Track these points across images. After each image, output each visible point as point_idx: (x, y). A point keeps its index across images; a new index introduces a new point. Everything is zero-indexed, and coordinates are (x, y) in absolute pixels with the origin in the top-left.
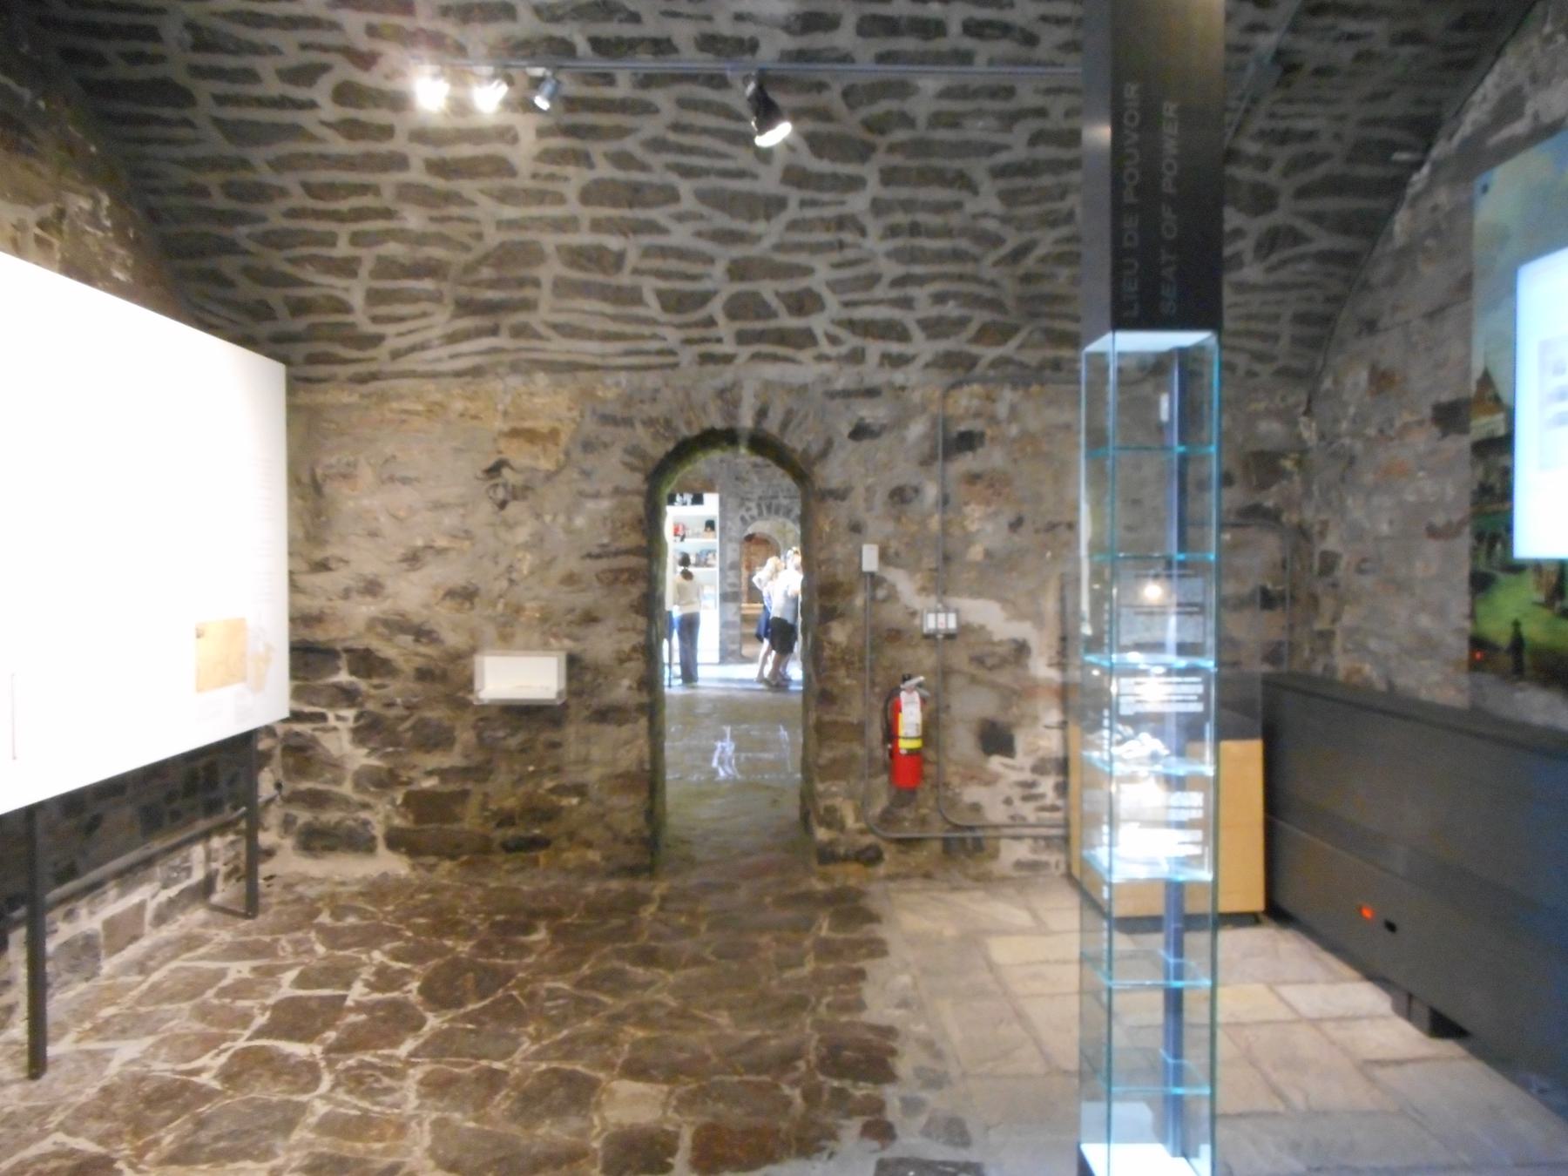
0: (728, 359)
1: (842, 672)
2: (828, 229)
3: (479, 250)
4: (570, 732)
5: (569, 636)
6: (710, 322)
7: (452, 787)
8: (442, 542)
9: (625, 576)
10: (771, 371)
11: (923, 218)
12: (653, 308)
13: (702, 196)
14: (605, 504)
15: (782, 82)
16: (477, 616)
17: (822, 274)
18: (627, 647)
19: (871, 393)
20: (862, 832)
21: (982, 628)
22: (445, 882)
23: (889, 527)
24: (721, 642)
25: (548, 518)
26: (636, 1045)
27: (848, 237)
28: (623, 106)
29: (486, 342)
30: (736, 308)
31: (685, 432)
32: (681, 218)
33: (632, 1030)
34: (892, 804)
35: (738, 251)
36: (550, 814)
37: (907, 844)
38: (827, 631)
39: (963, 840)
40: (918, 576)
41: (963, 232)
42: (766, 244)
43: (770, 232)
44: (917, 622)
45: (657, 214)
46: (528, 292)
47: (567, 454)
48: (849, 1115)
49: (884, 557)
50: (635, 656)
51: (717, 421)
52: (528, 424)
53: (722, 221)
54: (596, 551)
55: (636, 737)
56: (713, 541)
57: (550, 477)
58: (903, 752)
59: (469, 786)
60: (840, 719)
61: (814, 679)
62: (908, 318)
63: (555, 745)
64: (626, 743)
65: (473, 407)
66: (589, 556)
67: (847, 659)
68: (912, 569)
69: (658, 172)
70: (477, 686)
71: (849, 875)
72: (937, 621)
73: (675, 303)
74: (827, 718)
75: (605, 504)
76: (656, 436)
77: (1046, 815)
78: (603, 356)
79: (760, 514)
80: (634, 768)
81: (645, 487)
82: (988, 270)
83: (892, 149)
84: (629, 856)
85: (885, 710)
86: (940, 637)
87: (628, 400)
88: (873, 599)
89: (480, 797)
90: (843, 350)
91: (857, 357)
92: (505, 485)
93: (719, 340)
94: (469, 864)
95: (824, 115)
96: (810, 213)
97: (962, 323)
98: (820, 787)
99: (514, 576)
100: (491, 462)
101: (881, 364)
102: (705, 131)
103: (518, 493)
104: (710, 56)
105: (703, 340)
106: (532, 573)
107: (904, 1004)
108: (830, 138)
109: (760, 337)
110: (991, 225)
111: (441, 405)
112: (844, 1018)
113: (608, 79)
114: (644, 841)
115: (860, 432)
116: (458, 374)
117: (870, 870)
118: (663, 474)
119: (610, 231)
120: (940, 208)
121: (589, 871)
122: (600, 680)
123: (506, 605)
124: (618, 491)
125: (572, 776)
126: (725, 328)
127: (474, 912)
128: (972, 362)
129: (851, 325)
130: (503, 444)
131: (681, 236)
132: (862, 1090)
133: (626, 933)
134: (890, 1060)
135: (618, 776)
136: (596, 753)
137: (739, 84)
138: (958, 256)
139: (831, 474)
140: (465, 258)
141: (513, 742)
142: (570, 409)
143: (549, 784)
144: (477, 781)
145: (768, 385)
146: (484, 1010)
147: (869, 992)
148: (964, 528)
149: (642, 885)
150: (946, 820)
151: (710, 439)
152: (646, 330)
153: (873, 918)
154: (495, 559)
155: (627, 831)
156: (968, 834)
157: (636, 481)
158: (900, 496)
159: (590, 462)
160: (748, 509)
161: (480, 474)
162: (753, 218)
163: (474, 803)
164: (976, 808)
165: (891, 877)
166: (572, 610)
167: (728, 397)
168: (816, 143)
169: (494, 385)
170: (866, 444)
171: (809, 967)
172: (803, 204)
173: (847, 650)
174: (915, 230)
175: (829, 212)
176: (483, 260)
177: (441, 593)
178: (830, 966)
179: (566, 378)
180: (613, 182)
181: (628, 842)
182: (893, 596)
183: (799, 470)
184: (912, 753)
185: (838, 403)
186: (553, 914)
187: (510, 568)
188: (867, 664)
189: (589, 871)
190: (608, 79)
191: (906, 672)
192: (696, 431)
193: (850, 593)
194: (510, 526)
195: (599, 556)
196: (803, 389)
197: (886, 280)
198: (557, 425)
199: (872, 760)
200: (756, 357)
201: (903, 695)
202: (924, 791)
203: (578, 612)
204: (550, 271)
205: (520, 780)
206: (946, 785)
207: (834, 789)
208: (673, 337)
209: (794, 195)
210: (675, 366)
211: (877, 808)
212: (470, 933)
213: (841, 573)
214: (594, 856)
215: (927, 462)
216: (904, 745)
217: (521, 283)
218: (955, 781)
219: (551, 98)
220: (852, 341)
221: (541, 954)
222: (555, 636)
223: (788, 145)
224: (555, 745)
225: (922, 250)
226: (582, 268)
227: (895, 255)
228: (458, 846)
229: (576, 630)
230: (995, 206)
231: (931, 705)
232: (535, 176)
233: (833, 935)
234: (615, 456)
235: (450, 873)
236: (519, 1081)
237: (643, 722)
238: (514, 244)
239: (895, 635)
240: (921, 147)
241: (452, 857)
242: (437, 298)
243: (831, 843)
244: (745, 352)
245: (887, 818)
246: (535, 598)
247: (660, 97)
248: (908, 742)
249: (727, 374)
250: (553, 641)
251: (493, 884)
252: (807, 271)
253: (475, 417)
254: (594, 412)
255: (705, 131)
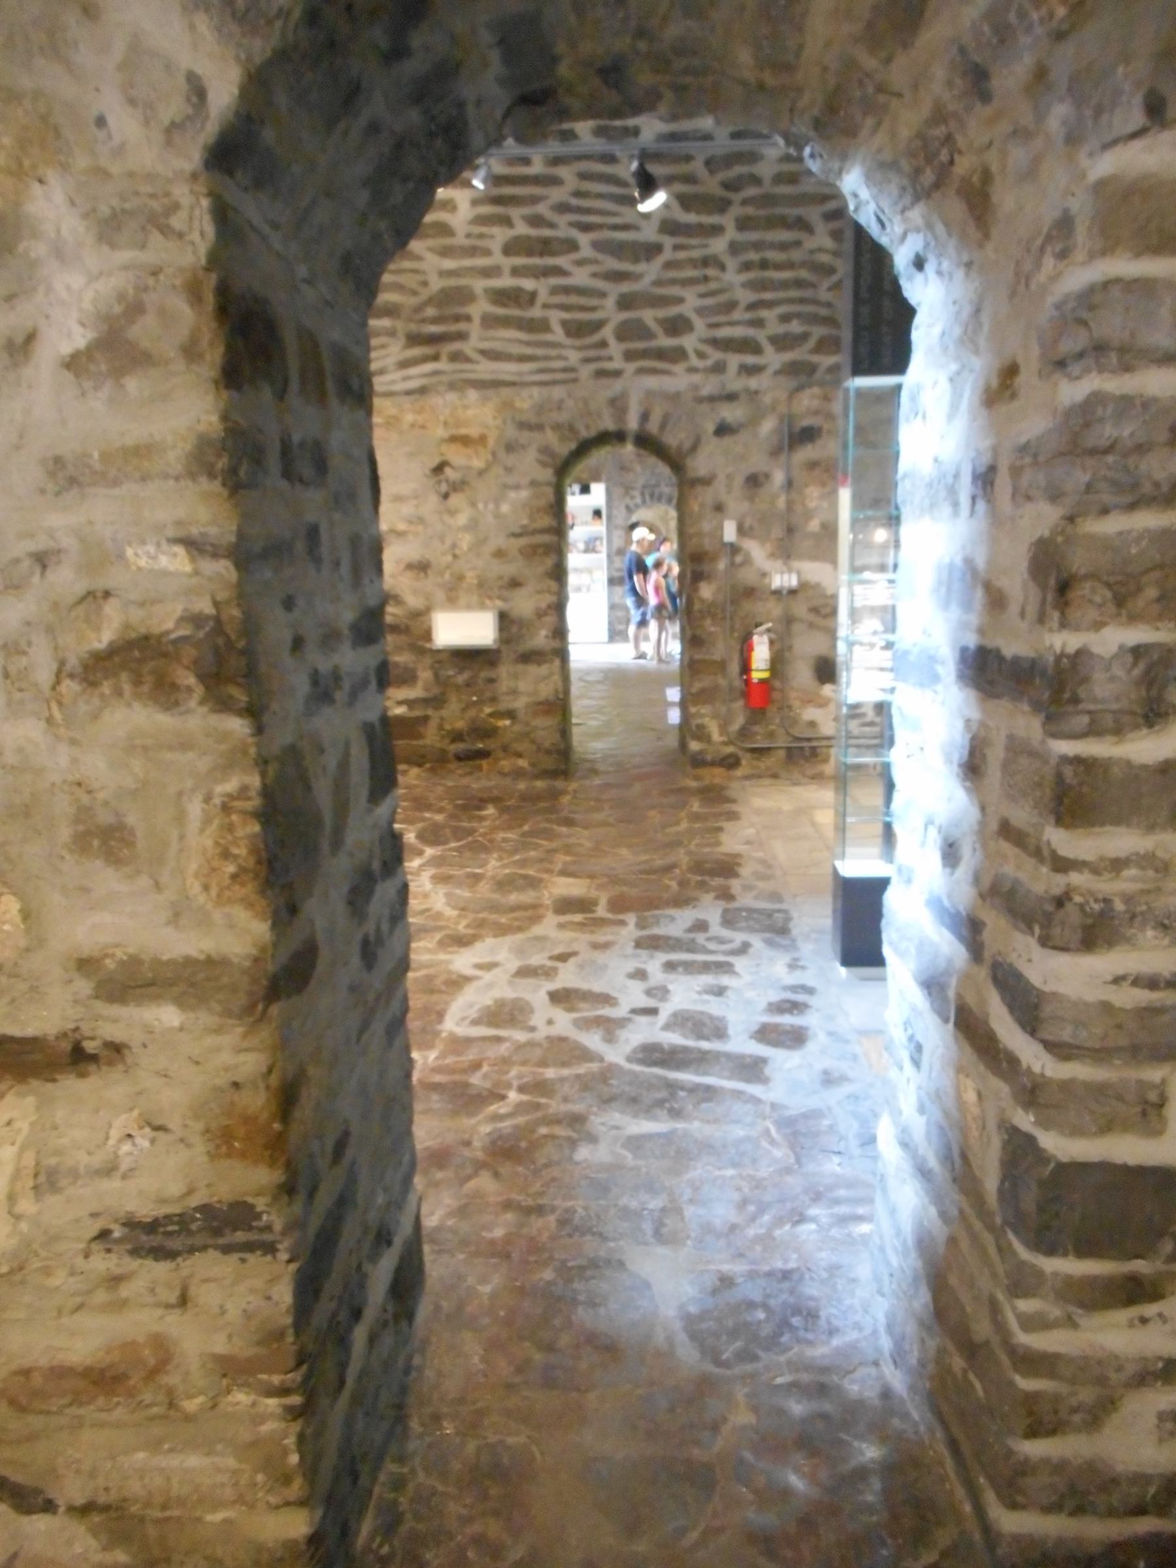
0: (617, 374)
1: (708, 622)
2: (695, 267)
3: (425, 294)
4: (504, 671)
5: (500, 598)
6: (603, 344)
7: (418, 713)
8: (402, 527)
9: (540, 551)
10: (652, 382)
11: (773, 255)
12: (558, 334)
13: (597, 245)
14: (524, 494)
15: (658, 157)
16: (429, 583)
17: (691, 302)
18: (543, 605)
19: (731, 397)
20: (725, 744)
21: (818, 585)
22: (415, 782)
23: (745, 506)
24: (610, 623)
25: (481, 506)
26: (565, 863)
27: (711, 272)
28: (536, 180)
29: (429, 367)
30: (625, 332)
31: (585, 434)
32: (580, 263)
33: (562, 857)
34: (747, 723)
35: (626, 287)
36: (488, 733)
37: (760, 752)
38: (696, 590)
39: (802, 748)
40: (768, 545)
41: (803, 264)
42: (647, 280)
43: (650, 270)
44: (767, 581)
45: (561, 261)
46: (462, 326)
47: (494, 454)
48: (707, 892)
49: (741, 531)
50: (549, 612)
51: (609, 424)
52: (463, 431)
53: (612, 264)
54: (518, 530)
55: (551, 674)
56: (600, 528)
57: (481, 473)
58: (755, 681)
59: (430, 712)
60: (707, 657)
61: (687, 628)
62: (761, 335)
63: (491, 681)
64: (545, 678)
65: (420, 419)
66: (514, 535)
67: (711, 611)
68: (763, 539)
69: (563, 229)
70: (434, 636)
71: (716, 775)
72: (782, 579)
73: (576, 330)
74: (697, 657)
75: (524, 494)
76: (562, 439)
77: (867, 729)
78: (520, 374)
79: (644, 502)
80: (552, 698)
81: (553, 479)
82: (824, 295)
83: (745, 202)
84: (549, 763)
85: (742, 651)
86: (785, 592)
87: (540, 409)
88: (732, 564)
89: (438, 720)
90: (709, 363)
91: (719, 368)
92: (447, 481)
93: (610, 359)
94: (432, 770)
95: (690, 179)
96: (682, 255)
97: (805, 337)
98: (693, 710)
99: (457, 552)
100: (435, 462)
101: (739, 373)
102: (600, 196)
103: (457, 487)
104: (603, 140)
105: (598, 359)
106: (470, 549)
107: (748, 843)
108: (696, 197)
109: (644, 354)
110: (825, 258)
111: (396, 418)
112: (707, 850)
113: (526, 161)
114: (558, 752)
115: (723, 430)
116: (408, 393)
117: (731, 773)
118: (566, 468)
119: (526, 276)
120: (783, 247)
121: (519, 774)
122: (524, 631)
123: (452, 574)
124: (533, 484)
125: (503, 706)
126: (615, 349)
127: (441, 799)
128: (812, 369)
129: (715, 343)
130: (444, 448)
131: (581, 277)
132: (718, 881)
133: (553, 810)
134: (736, 868)
135: (540, 703)
136: (522, 686)
137: (625, 161)
138: (799, 284)
139: (699, 465)
140: (412, 301)
141: (461, 679)
142: (495, 418)
143: (488, 710)
144: (436, 708)
145: (650, 394)
146: (462, 847)
147: (724, 837)
148: (804, 505)
149: (559, 784)
150: (788, 733)
151: (602, 438)
152: (553, 352)
153: (734, 801)
154: (442, 539)
155: (547, 744)
156: (805, 744)
157: (548, 475)
158: (754, 481)
159: (511, 460)
160: (632, 498)
161: (428, 472)
162: (636, 260)
163: (433, 724)
164: (812, 724)
165: (747, 778)
166: (501, 578)
167: (618, 404)
168: (685, 202)
169: (436, 400)
170: (727, 441)
171: (684, 825)
172: (676, 248)
173: (713, 604)
174: (764, 265)
175: (696, 254)
176: (430, 301)
177: (402, 566)
178: (698, 825)
179: (490, 393)
180: (528, 238)
181: (548, 752)
182: (748, 561)
183: (675, 462)
184: (763, 682)
185: (705, 408)
186: (495, 800)
187: (454, 546)
188: (728, 615)
189: (519, 774)
190: (526, 161)
191: (758, 620)
192: (593, 433)
193: (714, 559)
194: (452, 513)
195: (519, 535)
196: (675, 397)
197: (743, 305)
198: (485, 431)
199: (731, 689)
200: (641, 371)
201: (756, 638)
202: (772, 710)
203: (506, 579)
204: (480, 308)
205: (469, 705)
206: (790, 707)
207: (703, 711)
208: (574, 357)
209: (668, 241)
210: (575, 380)
211: (735, 727)
212: (440, 810)
213: (708, 544)
214: (522, 763)
215: (775, 452)
216: (756, 676)
217: (457, 318)
218: (796, 704)
219: (485, 182)
220: (716, 355)
221: (494, 821)
222: (490, 598)
223: (666, 206)
224: (491, 681)
225: (771, 281)
226: (504, 305)
227: (751, 285)
228: (423, 756)
229: (505, 593)
230: (828, 243)
231: (777, 646)
232: (468, 236)
233: (701, 810)
234: (532, 455)
235: (418, 777)
236: (493, 878)
237: (557, 662)
238: (451, 288)
239: (750, 592)
240: (768, 200)
241: (420, 765)
242: (392, 333)
243: (701, 752)
244: (631, 367)
245: (744, 733)
246: (474, 568)
247: (565, 172)
248: (759, 674)
249: (617, 386)
250: (488, 602)
251: (450, 784)
252: (680, 300)
253: (423, 427)
254: (513, 419)
255: (600, 196)
